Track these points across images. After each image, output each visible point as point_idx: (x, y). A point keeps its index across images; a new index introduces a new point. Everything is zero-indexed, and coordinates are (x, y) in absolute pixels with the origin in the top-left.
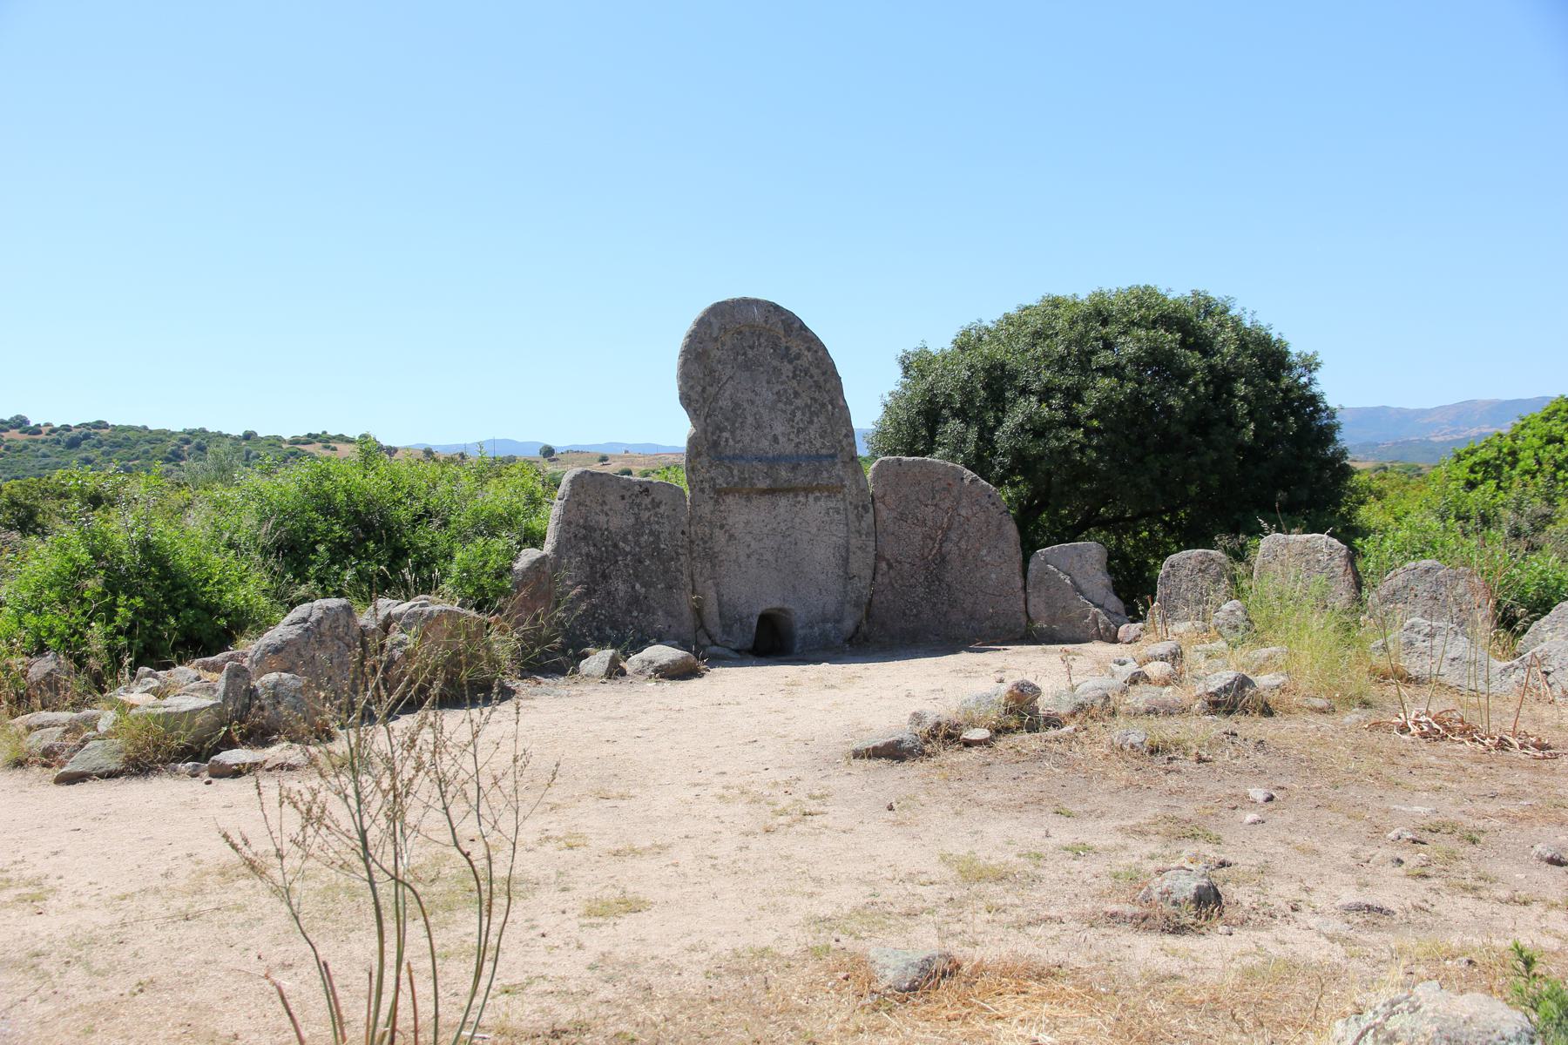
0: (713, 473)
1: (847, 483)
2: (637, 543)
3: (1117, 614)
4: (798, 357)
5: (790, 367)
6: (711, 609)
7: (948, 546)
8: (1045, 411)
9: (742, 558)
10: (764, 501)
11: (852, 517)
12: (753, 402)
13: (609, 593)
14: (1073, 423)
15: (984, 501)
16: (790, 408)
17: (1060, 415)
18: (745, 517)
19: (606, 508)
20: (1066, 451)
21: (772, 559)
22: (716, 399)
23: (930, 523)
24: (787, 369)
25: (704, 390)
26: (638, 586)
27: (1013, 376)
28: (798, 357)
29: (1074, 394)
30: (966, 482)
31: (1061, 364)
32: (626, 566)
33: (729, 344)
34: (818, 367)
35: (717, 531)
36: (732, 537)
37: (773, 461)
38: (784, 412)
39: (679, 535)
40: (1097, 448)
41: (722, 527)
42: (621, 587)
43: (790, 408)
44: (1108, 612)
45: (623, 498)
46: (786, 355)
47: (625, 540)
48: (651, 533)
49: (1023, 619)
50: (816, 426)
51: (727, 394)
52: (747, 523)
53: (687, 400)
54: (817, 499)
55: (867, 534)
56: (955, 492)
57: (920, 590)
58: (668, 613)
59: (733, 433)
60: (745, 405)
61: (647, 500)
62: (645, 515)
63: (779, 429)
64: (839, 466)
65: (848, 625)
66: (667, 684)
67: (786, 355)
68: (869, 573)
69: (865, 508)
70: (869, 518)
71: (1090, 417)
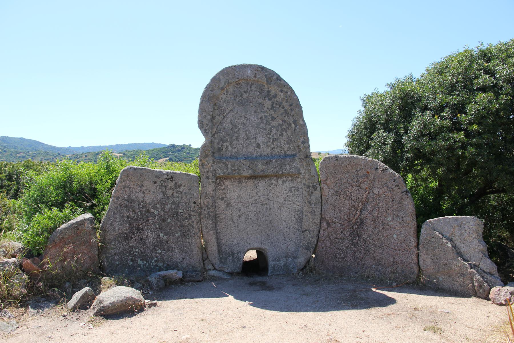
0: (215, 167)
1: (302, 172)
2: (163, 209)
3: (491, 274)
4: (275, 96)
5: (270, 102)
6: (213, 248)
7: (365, 214)
8: (438, 121)
9: (235, 218)
10: (250, 183)
11: (305, 193)
12: (245, 124)
13: (141, 239)
14: (456, 127)
15: (391, 184)
16: (268, 127)
17: (447, 123)
18: (234, 191)
19: (143, 189)
20: (450, 149)
21: (254, 218)
22: (221, 123)
23: (354, 198)
24: (268, 103)
25: (213, 118)
26: (162, 235)
27: (419, 99)
28: (275, 96)
29: (459, 108)
30: (379, 171)
31: (452, 88)
32: (155, 223)
33: (231, 91)
34: (287, 102)
35: (219, 202)
36: (229, 204)
37: (252, 159)
38: (265, 129)
39: (192, 204)
40: (477, 146)
41: (222, 199)
42: (150, 235)
43: (268, 127)
44: (482, 273)
45: (155, 182)
46: (268, 96)
47: (155, 207)
48: (173, 203)
49: (416, 269)
50: (285, 137)
51: (229, 120)
52: (239, 196)
53: (201, 125)
54: (284, 182)
55: (316, 204)
56: (371, 177)
57: (346, 242)
58: (182, 251)
59: (231, 143)
60: (240, 126)
61: (172, 184)
62: (170, 193)
63: (261, 139)
64: (297, 161)
65: (301, 261)
66: (104, 321)
67: (268, 96)
68: (316, 228)
69: (314, 187)
70: (317, 194)
71: (470, 123)
